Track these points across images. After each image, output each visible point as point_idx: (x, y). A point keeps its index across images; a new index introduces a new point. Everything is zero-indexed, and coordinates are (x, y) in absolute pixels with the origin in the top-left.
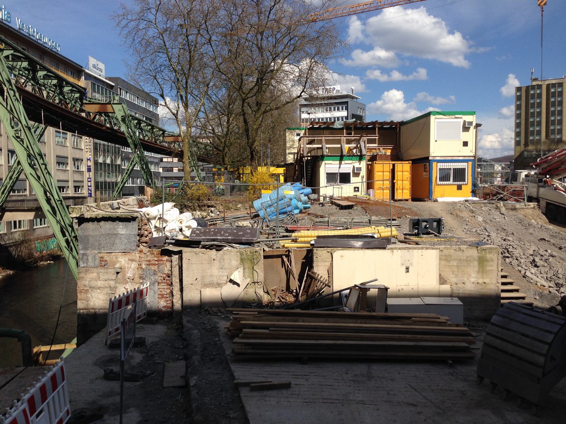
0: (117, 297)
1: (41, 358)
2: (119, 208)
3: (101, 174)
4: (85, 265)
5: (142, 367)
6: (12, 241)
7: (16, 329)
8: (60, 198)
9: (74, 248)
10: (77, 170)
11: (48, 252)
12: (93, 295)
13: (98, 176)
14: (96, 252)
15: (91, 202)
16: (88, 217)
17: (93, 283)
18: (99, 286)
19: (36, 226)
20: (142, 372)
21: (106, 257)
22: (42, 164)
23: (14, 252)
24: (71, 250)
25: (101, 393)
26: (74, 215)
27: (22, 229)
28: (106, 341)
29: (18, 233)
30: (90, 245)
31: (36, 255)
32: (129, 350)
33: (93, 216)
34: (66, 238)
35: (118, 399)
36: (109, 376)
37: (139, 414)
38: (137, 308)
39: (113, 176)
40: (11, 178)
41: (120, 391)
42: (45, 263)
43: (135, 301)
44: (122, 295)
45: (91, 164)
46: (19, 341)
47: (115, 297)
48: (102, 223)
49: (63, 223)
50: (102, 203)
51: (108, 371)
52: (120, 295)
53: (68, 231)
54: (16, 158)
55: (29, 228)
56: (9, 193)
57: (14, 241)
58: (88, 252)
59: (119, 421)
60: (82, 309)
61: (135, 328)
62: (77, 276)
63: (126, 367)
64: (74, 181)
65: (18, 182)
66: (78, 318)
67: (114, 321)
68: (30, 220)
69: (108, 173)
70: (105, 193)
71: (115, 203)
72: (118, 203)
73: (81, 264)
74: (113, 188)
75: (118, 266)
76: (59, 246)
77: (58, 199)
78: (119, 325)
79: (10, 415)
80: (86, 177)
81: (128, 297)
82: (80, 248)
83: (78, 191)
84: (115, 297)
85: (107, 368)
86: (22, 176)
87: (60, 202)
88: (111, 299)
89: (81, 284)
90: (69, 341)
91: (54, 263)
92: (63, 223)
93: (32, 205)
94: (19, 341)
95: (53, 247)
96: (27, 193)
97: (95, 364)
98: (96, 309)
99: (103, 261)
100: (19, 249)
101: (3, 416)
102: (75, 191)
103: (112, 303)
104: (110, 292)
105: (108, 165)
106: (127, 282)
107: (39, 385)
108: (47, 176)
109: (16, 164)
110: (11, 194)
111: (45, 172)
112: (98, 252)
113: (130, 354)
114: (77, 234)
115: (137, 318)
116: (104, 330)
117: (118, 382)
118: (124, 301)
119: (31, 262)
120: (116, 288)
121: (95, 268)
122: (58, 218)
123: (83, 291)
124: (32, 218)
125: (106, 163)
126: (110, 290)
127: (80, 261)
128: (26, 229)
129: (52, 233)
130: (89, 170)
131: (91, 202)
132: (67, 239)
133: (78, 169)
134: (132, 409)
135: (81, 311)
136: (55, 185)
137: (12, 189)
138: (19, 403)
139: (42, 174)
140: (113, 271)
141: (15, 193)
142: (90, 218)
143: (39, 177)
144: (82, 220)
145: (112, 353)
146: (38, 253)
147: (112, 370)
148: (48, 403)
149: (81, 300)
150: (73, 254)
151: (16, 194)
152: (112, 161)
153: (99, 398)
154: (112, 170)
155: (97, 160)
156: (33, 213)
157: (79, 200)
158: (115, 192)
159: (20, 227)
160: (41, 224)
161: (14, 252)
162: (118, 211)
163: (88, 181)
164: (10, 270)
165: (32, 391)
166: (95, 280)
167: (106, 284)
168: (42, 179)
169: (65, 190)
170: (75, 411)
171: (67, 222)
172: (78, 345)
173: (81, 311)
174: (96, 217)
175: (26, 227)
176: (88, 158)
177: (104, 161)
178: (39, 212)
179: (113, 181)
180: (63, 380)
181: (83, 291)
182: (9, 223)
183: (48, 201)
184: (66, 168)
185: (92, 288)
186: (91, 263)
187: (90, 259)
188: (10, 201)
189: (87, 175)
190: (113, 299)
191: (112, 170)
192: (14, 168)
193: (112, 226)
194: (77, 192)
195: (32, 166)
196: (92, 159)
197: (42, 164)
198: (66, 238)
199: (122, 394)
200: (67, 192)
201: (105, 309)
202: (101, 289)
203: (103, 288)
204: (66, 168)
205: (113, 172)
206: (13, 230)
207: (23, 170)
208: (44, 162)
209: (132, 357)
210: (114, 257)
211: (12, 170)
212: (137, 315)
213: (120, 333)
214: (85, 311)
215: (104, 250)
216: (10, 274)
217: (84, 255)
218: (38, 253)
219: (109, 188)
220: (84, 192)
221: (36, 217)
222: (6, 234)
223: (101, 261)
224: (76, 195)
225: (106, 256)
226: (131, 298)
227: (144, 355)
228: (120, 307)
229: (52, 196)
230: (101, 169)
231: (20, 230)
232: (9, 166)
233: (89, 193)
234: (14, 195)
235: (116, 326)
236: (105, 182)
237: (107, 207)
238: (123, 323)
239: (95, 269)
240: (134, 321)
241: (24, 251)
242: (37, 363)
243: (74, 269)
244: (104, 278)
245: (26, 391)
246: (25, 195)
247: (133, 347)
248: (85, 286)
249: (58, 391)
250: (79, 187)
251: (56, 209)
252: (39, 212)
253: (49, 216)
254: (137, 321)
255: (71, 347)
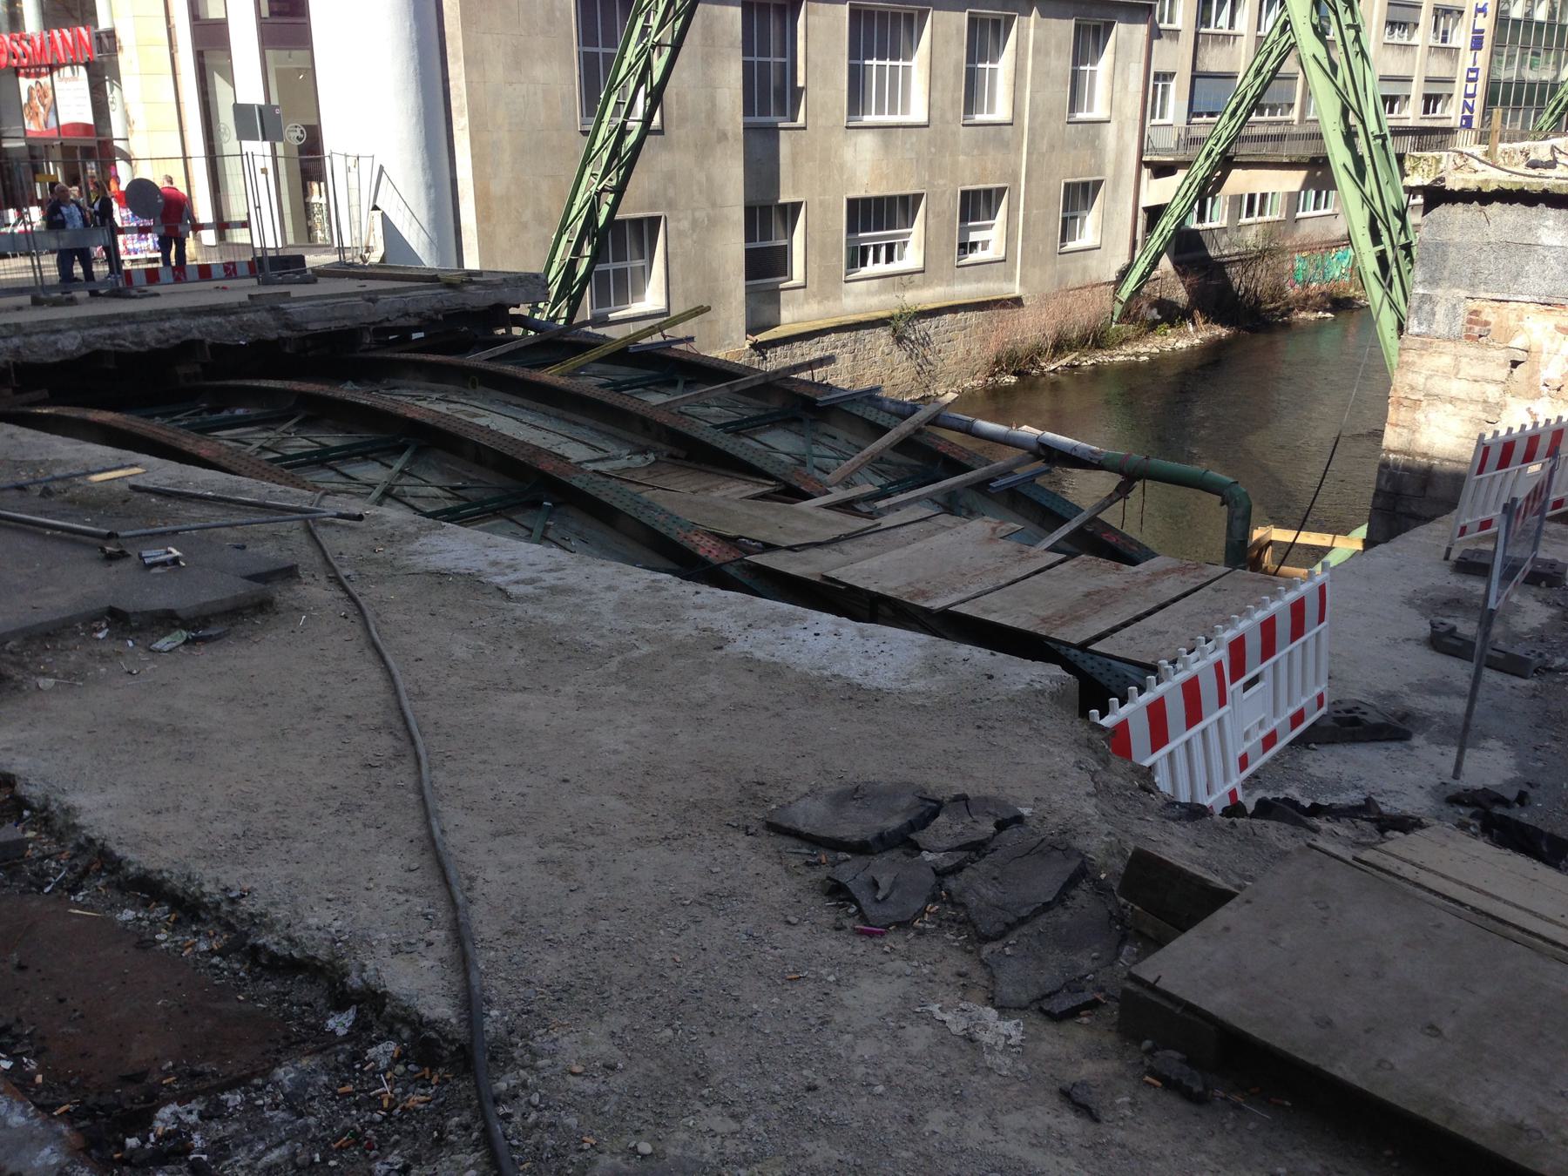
0: (1503, 433)
1: (1267, 557)
2: (1552, 164)
3: (1511, 57)
4: (1424, 329)
5: (1542, 641)
6: (1237, 250)
7: (1218, 475)
8: (1381, 130)
9: (1396, 280)
10: (1440, 44)
11: (1324, 288)
12: (1431, 416)
13: (1500, 62)
14: (1463, 294)
15: (1466, 142)
16: (1456, 189)
17: (1439, 385)
18: (1453, 393)
19: (1304, 210)
20: (1540, 655)
21: (1489, 314)
22: (1349, 26)
23: (1237, 280)
24: (1390, 286)
25: (1414, 680)
26: (1415, 180)
27: (1267, 218)
28: (1449, 550)
29: (1254, 229)
30: (1446, 274)
31: (1292, 292)
32: (1512, 585)
33: (1472, 186)
34: (1381, 247)
35: (1459, 706)
36: (1442, 642)
37: (1513, 762)
38: (1557, 474)
39: (1547, 63)
40: (1258, 72)
41: (1468, 688)
42: (1312, 316)
43: (1553, 452)
44: (1516, 430)
45: (1486, 23)
46: (1222, 504)
47: (1496, 433)
48: (1495, 208)
49: (1378, 205)
50: (1502, 146)
51: (1442, 629)
52: (1510, 429)
53: (1389, 230)
54: (1278, 12)
55: (1284, 217)
56: (1249, 115)
57: (1243, 250)
58: (1439, 292)
59: (1453, 761)
60: (1394, 452)
61: (1539, 531)
62: (1395, 360)
63: (1497, 629)
64: (1428, 81)
65: (1275, 82)
66: (1380, 473)
67: (1481, 497)
68: (1290, 194)
69: (1534, 54)
70: (1514, 119)
71: (1542, 151)
72: (1553, 148)
73: (1413, 326)
74: (1541, 101)
75: (1519, 342)
76: (1356, 272)
77: (1377, 133)
78: (1495, 514)
79: (1186, 667)
80: (1463, 65)
81: (1533, 440)
82: (1418, 279)
83: (1434, 111)
84: (1496, 433)
85: (1440, 619)
86: (1290, 66)
87: (1379, 141)
88: (1482, 436)
89: (1402, 382)
90: (1346, 531)
91: (1334, 320)
92: (1378, 205)
93: (1305, 151)
94: (1222, 504)
95: (1337, 274)
96: (1294, 115)
97: (1410, 602)
98: (1433, 458)
99: (1476, 323)
100: (1250, 274)
101: (1170, 663)
102: (1426, 111)
103: (1484, 449)
104: (1483, 416)
105: (1540, 25)
106: (1539, 396)
107: (1260, 615)
108: (1357, 63)
109: (1277, 31)
110: (1254, 117)
111: (1353, 49)
112: (1468, 294)
113: (1514, 599)
114: (1411, 237)
115: (1550, 505)
116: (1446, 518)
117: (1467, 663)
118: (1520, 450)
119: (1276, 309)
120: (1501, 406)
121: (1449, 340)
122: (1367, 191)
123: (1406, 403)
124: (1296, 187)
125: (1531, 22)
126: (1484, 411)
127: (1412, 316)
128: (1277, 217)
129: (1345, 232)
130: (1477, 44)
131: (1466, 142)
132: (1383, 252)
133: (1444, 40)
134: (1491, 743)
135: (1392, 456)
136: (1375, 89)
137: (1257, 106)
138: (1193, 656)
139: (1343, 57)
140: (1502, 356)
141: (1262, 114)
142: (1462, 191)
143: (1334, 67)
144: (1436, 196)
145: (1460, 585)
146: (1297, 286)
147: (1454, 629)
148: (1275, 664)
149: (1397, 425)
150: (1394, 296)
151: (1266, 117)
152: (1552, 15)
153: (1406, 689)
154: (1549, 43)
155: (1507, 12)
156: (1302, 174)
157: (1432, 137)
158: (1547, 115)
159: (1261, 213)
160: (1316, 208)
161: (1237, 280)
162: (1548, 172)
163: (1469, 80)
164: (1222, 326)
165: (1243, 625)
166: (1446, 376)
167: (1475, 390)
168: (1343, 71)
169: (1396, 106)
170: (1340, 702)
171: (1391, 201)
172: (1369, 543)
173: (1392, 456)
174: (1479, 189)
175: (1275, 214)
176: (1480, 6)
177: (1527, 14)
178: (1318, 172)
179: (1544, 78)
180: (1321, 619)
181: (1406, 403)
182: (1236, 200)
183: (1349, 137)
184: (1409, 38)
185: (1432, 396)
186: (1440, 326)
187: (1440, 311)
188: (1247, 138)
189: (1466, 59)
190: (1489, 436)
191: (1549, 43)
192: (1269, 41)
193: (1521, 220)
194: (1431, 115)
195: (1320, 32)
196: (1491, 10)
197: (1349, 26)
198: (1381, 247)
199: (1472, 697)
200: (1403, 114)
201: (1459, 462)
202: (1458, 403)
203: (1464, 401)
204: (1409, 38)
205: (1548, 50)
206: (1244, 220)
207: (1293, 45)
208: (1354, 20)
209: (1517, 609)
210: (1513, 316)
211: (1266, 47)
212: (1554, 497)
213: (1495, 537)
214: (1401, 458)
215: (1487, 291)
216: (1220, 336)
217: (1425, 298)
218: (1297, 286)
219: (1529, 102)
220: (1451, 114)
221: (1306, 186)
222: (1223, 230)
223: (1470, 321)
224: (1427, 123)
225: (1488, 310)
226: (1544, 444)
227: (1554, 611)
228: (1504, 462)
229: (1363, 122)
230: (1514, 41)
231: (1260, 219)
232: (1259, 38)
233: (1463, 118)
234: (1261, 123)
235: (1483, 513)
236: (1520, 83)
237: (1516, 160)
238: (1510, 509)
239: (1450, 345)
240: (1541, 511)
241: (1261, 280)
242: (1256, 565)
243: (1388, 341)
244: (1473, 372)
245: (1228, 622)
246: (1287, 122)
247: (1525, 582)
248: (1412, 388)
249: (1304, 644)
250: (1437, 98)
251: (1368, 161)
252: (1318, 172)
253: (1344, 181)
254: (1549, 514)
255: (1346, 546)
